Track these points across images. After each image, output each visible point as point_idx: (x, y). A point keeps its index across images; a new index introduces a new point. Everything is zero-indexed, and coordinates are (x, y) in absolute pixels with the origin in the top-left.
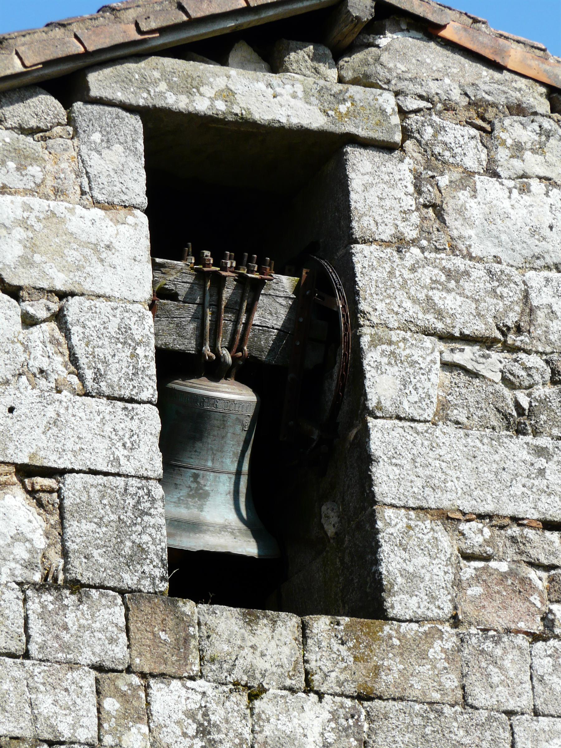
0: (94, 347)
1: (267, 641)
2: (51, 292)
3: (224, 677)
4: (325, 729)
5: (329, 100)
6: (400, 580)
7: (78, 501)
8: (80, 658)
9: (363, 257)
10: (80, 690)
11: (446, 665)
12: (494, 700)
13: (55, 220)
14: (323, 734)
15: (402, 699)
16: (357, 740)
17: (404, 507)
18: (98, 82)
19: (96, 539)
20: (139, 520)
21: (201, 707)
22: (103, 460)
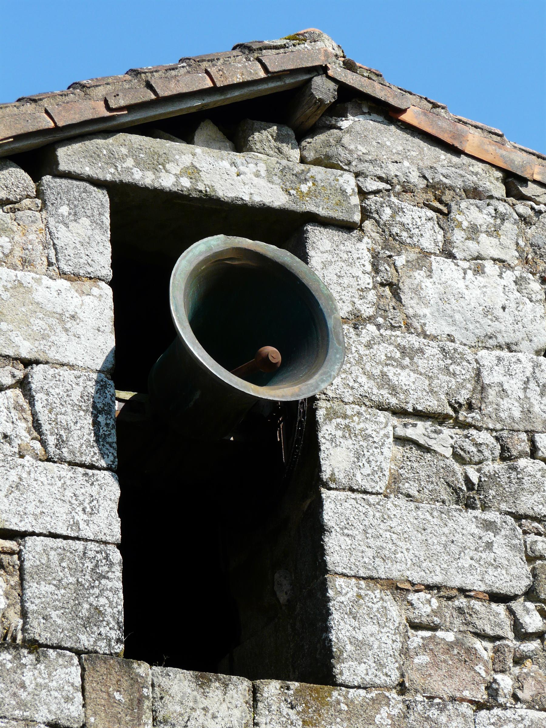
2: (16, 359)
5: (291, 179)
6: (349, 647)
8: (36, 716)
17: (354, 576)
18: (67, 157)
19: (54, 601)
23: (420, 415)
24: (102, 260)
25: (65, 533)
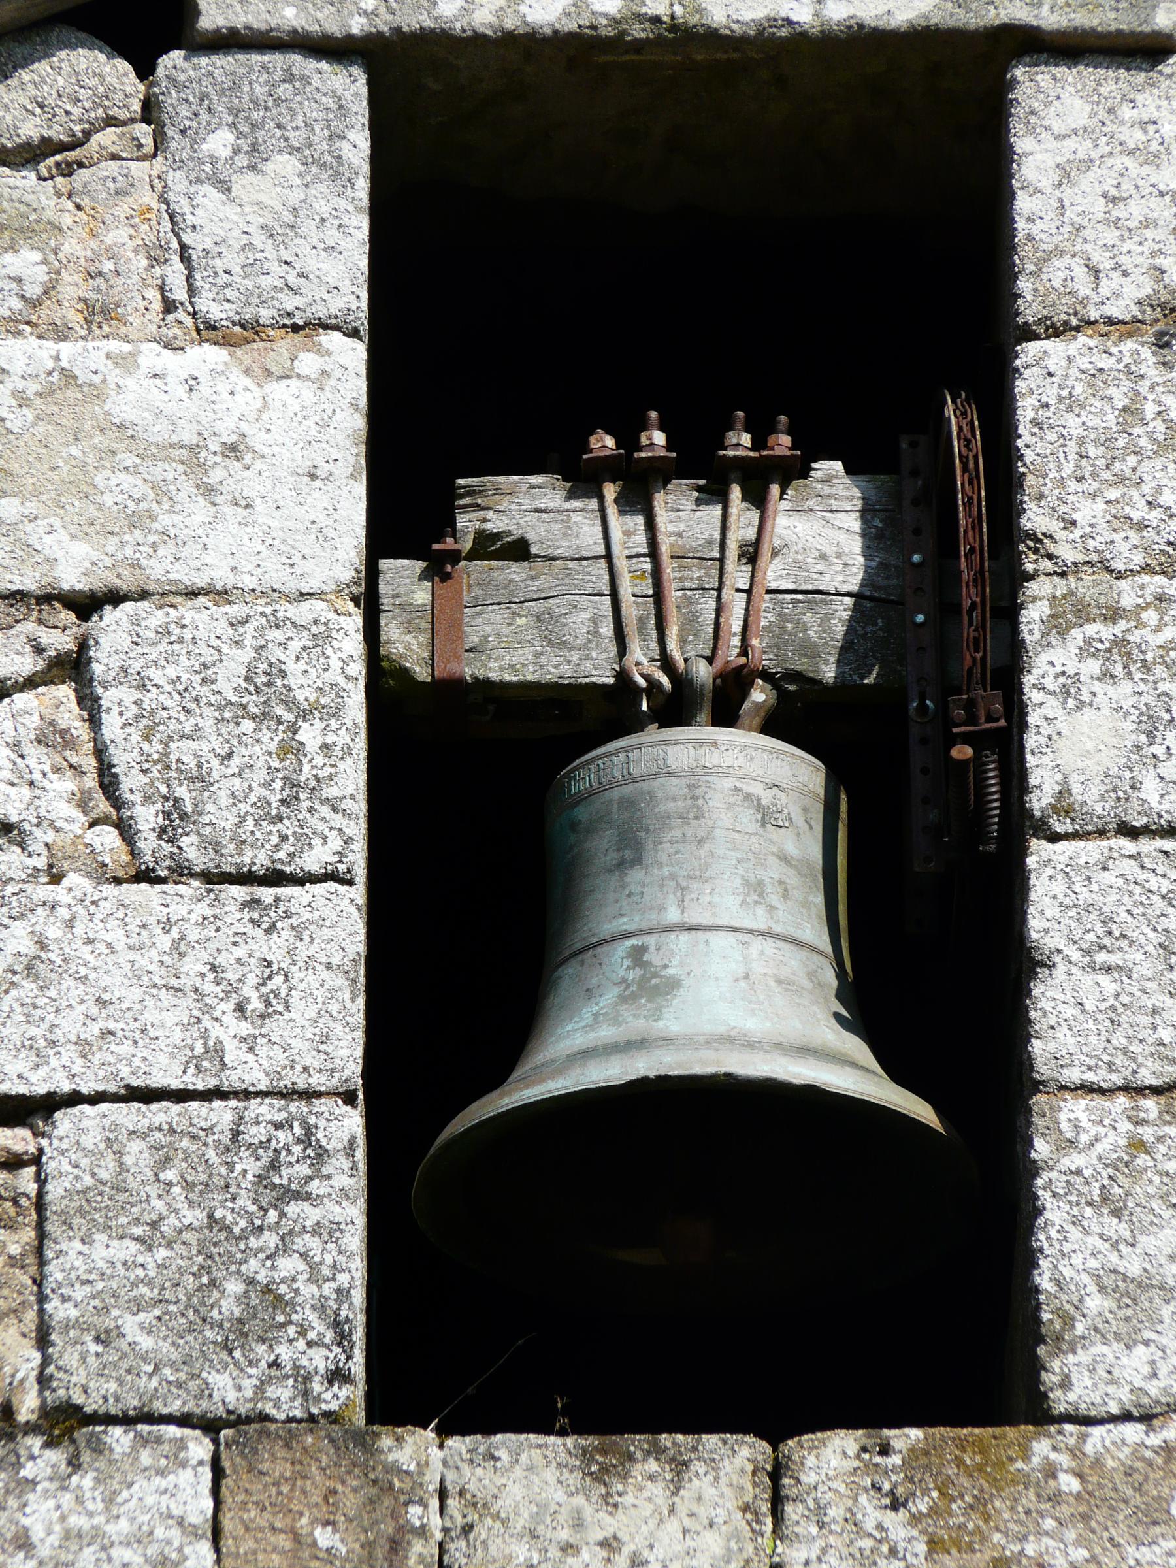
0: (171, 738)
6: (1095, 1303)
7: (88, 1181)
9: (1044, 375)
13: (72, 394)
17: (1125, 1089)
19: (134, 1285)
24: (337, 264)
25: (176, 1084)
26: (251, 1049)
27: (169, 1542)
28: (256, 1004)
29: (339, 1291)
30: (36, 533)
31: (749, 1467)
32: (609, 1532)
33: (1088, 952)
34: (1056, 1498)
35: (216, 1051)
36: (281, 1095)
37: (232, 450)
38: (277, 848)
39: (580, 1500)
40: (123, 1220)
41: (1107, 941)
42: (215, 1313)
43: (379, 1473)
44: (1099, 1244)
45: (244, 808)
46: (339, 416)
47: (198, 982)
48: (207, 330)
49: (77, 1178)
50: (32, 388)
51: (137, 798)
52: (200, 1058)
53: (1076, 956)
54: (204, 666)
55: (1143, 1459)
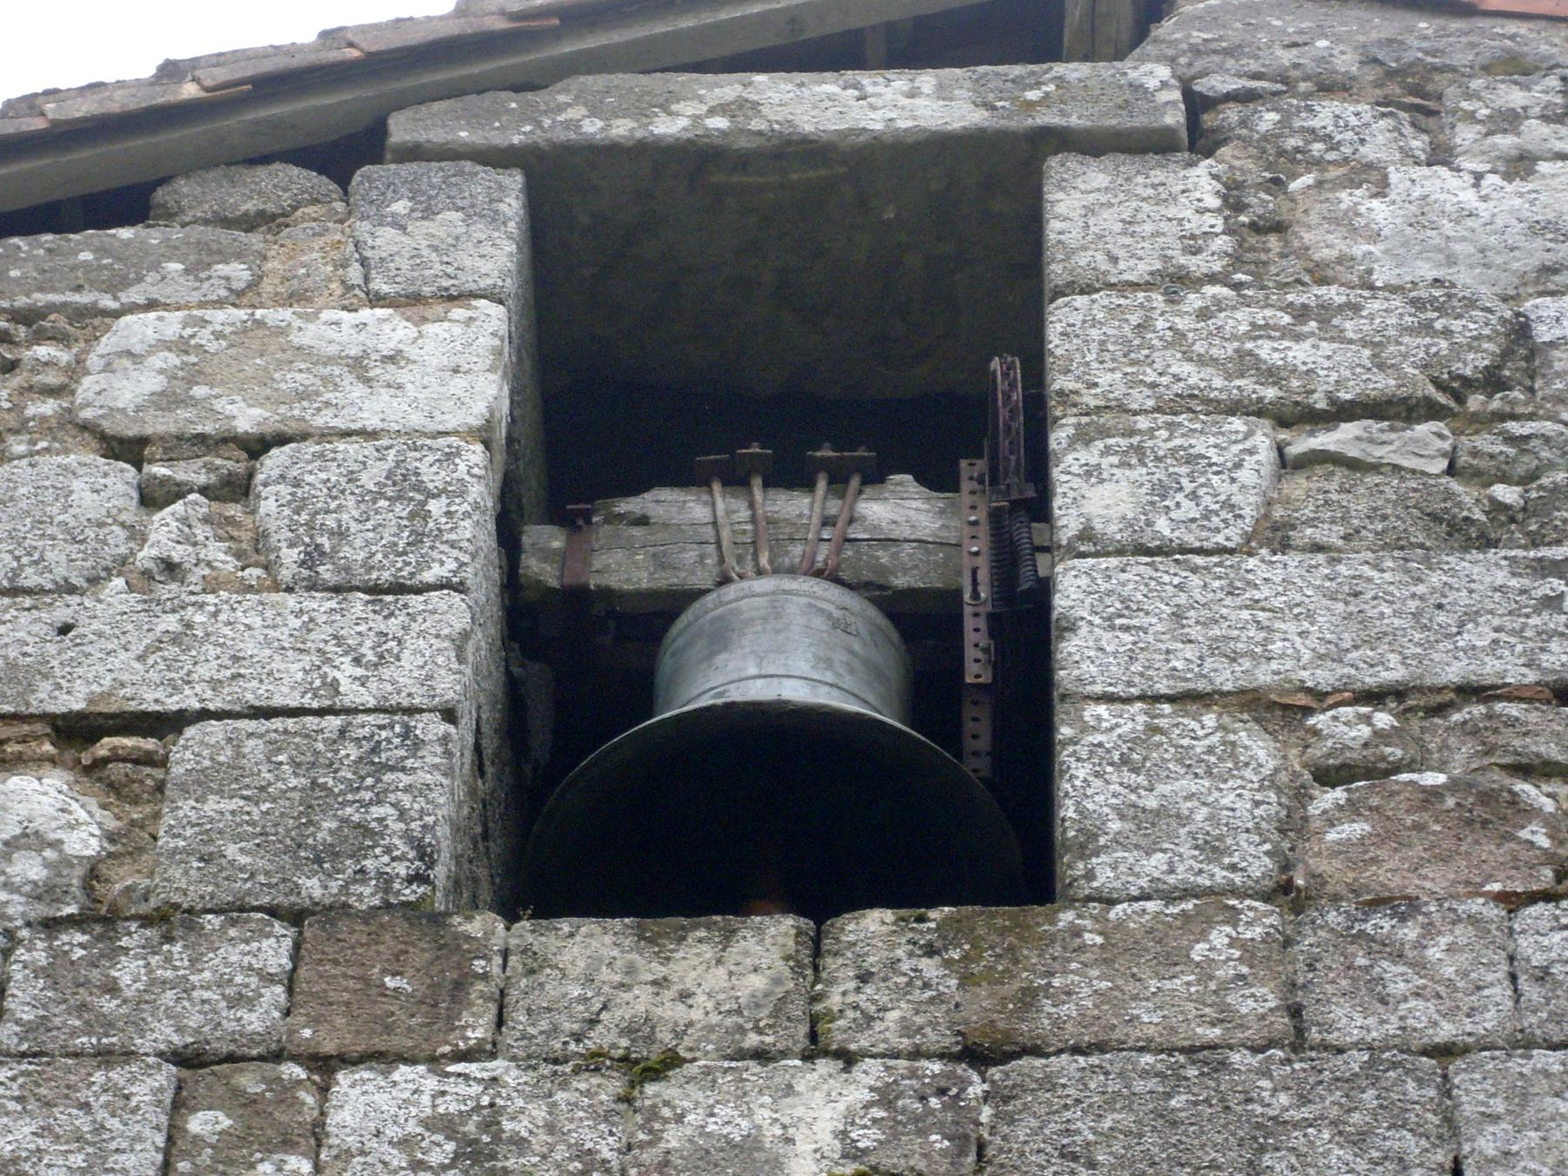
0: (317, 513)
1: (700, 969)
2: (225, 441)
3: (558, 1046)
4: (853, 1123)
6: (1115, 825)
7: (207, 763)
8: (139, 1041)
10: (121, 1103)
11: (1245, 970)
12: (1391, 1029)
13: (260, 333)
14: (845, 1133)
15: (1101, 1047)
16: (945, 1136)
17: (1142, 698)
19: (239, 825)
20: (369, 781)
21: (478, 1108)
22: (292, 688)
23: (1341, 412)
25: (294, 704)
26: (363, 685)
27: (247, 986)
28: (371, 657)
29: (424, 826)
30: (218, 405)
31: (793, 931)
32: (659, 976)
33: (1109, 619)
34: (1082, 948)
35: (334, 685)
36: (385, 711)
37: (391, 359)
38: (400, 570)
39: (635, 956)
40: (234, 786)
41: (1126, 612)
42: (310, 841)
43: (448, 939)
44: (1119, 789)
45: (374, 548)
46: (481, 339)
47: (322, 645)
48: (376, 300)
49: (198, 763)
50: (228, 330)
51: (284, 544)
52: (318, 689)
53: (1097, 620)
54: (352, 472)
55: (1164, 923)
